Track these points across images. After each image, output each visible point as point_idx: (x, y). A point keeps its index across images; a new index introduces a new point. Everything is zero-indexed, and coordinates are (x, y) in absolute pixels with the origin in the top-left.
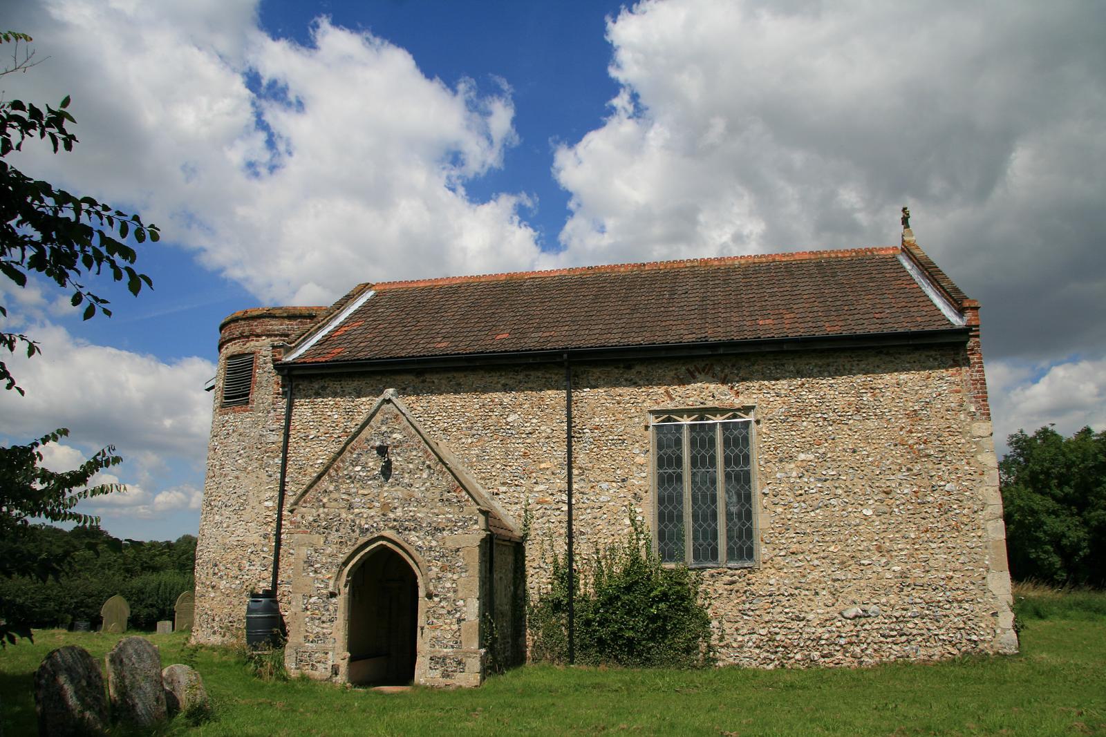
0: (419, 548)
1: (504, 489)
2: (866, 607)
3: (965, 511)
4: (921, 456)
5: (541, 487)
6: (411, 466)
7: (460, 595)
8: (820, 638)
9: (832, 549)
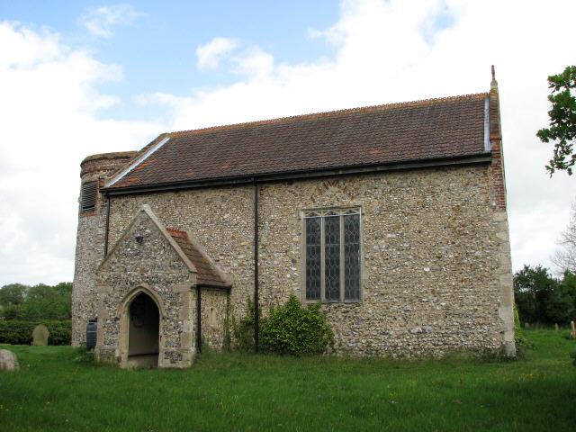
0: (159, 293)
1: (222, 257)
2: (424, 327)
4: (461, 234)
5: (242, 256)
8: (397, 346)
9: (405, 292)
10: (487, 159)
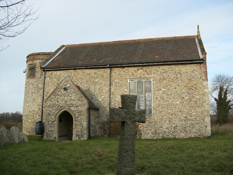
2: (177, 125)
3: (201, 103)
5: (103, 97)
6: (71, 92)
7: (82, 121)
10: (202, 61)
